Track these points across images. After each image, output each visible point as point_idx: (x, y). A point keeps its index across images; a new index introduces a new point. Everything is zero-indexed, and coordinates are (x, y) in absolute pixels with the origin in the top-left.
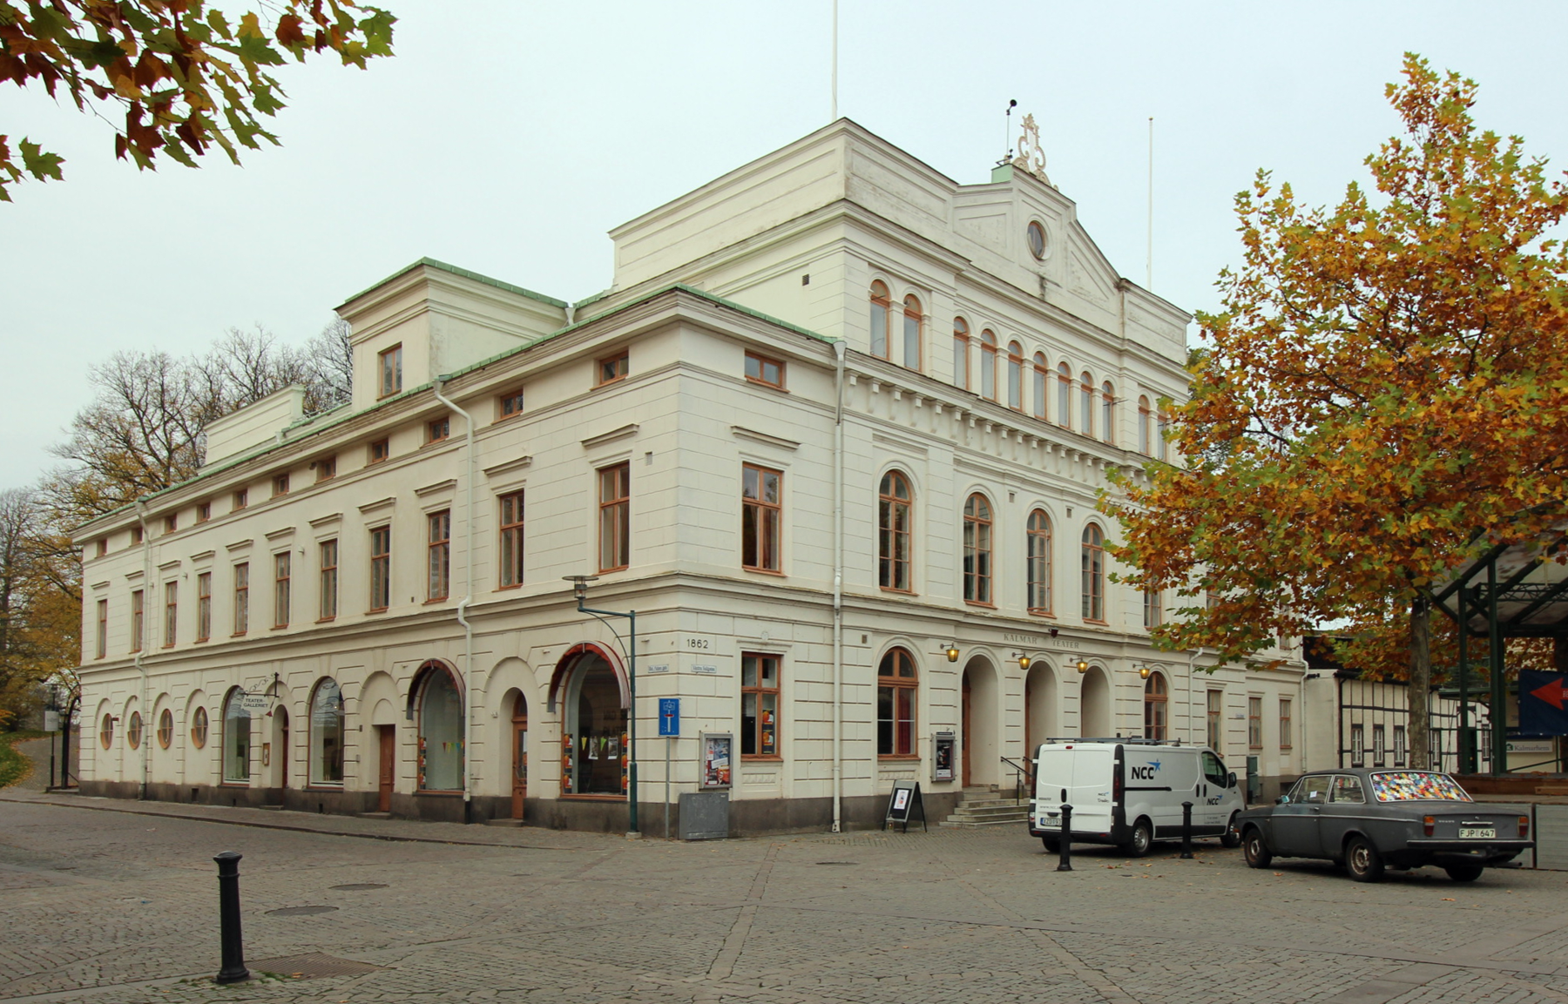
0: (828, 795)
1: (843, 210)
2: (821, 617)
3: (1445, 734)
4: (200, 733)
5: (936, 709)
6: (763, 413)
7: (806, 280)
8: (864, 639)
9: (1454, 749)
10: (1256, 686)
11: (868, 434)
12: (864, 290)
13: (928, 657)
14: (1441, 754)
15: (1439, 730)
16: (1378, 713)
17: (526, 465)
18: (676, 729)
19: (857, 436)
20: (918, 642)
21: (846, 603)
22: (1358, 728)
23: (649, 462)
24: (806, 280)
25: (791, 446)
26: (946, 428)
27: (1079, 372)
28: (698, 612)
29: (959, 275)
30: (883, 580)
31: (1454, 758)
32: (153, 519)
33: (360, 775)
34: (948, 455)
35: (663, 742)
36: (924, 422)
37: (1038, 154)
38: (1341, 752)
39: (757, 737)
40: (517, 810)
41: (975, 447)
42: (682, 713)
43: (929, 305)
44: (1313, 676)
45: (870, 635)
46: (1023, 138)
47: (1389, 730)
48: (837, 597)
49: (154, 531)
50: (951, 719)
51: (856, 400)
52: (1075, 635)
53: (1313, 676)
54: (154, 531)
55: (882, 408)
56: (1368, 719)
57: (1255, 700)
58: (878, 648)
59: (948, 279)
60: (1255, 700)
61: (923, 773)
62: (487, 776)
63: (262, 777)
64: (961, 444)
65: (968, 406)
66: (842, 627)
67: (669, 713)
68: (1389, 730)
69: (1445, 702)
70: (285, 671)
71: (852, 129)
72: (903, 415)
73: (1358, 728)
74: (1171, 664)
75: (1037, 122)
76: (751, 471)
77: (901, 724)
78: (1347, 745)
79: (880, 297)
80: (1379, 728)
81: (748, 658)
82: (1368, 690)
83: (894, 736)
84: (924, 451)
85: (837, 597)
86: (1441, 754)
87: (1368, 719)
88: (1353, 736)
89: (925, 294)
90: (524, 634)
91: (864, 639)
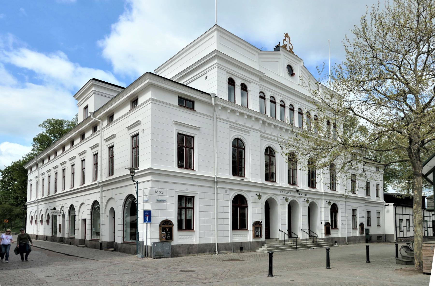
0: (214, 242)
1: (215, 54)
2: (344, 200)
3: (428, 222)
4: (48, 221)
5: (255, 213)
6: (184, 116)
7: (206, 78)
8: (226, 192)
9: (431, 226)
10: (369, 209)
11: (227, 126)
12: (226, 81)
13: (250, 198)
14: (427, 228)
15: (427, 221)
16: (401, 216)
17: (115, 137)
18: (150, 220)
19: (223, 127)
20: (247, 193)
21: (218, 180)
22: (401, 220)
23: (144, 133)
24: (206, 78)
25: (197, 129)
26: (257, 126)
27: (313, 116)
28: (174, 183)
29: (261, 79)
30: (309, 186)
31: (432, 229)
32: (39, 162)
33: (78, 236)
34: (258, 135)
35: (145, 224)
36: (249, 124)
37: (290, 45)
38: (396, 227)
39: (187, 225)
40: (112, 247)
41: (268, 132)
42: (152, 215)
43: (250, 87)
44: (387, 205)
45: (228, 191)
46: (285, 40)
47: (405, 221)
48: (215, 178)
49: (40, 165)
50: (261, 218)
51: (224, 115)
52: (305, 193)
53: (387, 205)
54: (40, 165)
55: (233, 119)
56: (405, 218)
57: (368, 213)
58: (232, 195)
59: (258, 80)
60: (368, 213)
61: (247, 236)
62: (105, 237)
63: (59, 235)
64: (263, 131)
65: (265, 119)
66: (217, 188)
67: (148, 215)
68: (405, 221)
69: (428, 212)
70: (64, 202)
71: (219, 29)
72: (241, 121)
73: (401, 220)
74: (339, 201)
75: (289, 35)
76: (180, 135)
77: (240, 220)
78: (398, 225)
79: (231, 82)
80: (408, 220)
81: (180, 198)
82: (404, 209)
83: (239, 223)
84: (249, 133)
85: (215, 178)
86: (427, 228)
87: (405, 218)
88: (400, 223)
89: (249, 83)
90: (114, 190)
91: (226, 192)
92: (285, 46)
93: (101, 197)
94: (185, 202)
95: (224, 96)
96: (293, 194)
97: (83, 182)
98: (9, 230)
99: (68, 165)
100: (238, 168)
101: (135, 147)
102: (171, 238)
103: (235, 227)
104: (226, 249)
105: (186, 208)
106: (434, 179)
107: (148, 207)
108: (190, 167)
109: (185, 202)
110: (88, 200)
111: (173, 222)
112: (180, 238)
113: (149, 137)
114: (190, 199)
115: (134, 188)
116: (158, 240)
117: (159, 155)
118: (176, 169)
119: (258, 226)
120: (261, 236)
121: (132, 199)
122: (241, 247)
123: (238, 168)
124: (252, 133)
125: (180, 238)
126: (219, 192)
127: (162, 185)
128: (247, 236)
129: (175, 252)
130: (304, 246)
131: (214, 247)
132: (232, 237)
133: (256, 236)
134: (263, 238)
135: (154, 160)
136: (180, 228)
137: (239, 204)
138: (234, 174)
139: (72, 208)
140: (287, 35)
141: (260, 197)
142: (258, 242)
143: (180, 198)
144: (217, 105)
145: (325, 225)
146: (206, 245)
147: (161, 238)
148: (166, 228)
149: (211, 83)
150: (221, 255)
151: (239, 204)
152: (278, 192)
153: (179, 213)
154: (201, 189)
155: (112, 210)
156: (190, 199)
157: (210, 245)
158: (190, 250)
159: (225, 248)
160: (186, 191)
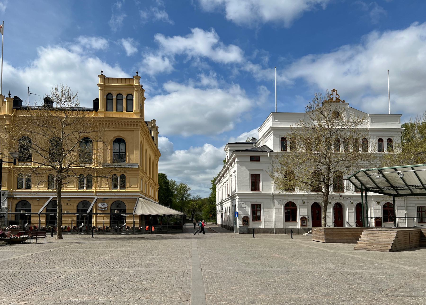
13: (346, 203)
39: (257, 218)
91: (280, 201)
95: (277, 150)
98: (205, 81)
109: (256, 208)
111: (249, 217)
112: (252, 225)
116: (242, 225)
118: (249, 192)
119: (304, 219)
120: (307, 226)
122: (292, 232)
125: (252, 225)
126: (275, 201)
129: (253, 231)
132: (285, 225)
136: (253, 220)
141: (352, 203)
142: (305, 229)
145: (375, 220)
147: (243, 224)
148: (245, 220)
157: (271, 229)
159: (279, 231)
160: (256, 202)
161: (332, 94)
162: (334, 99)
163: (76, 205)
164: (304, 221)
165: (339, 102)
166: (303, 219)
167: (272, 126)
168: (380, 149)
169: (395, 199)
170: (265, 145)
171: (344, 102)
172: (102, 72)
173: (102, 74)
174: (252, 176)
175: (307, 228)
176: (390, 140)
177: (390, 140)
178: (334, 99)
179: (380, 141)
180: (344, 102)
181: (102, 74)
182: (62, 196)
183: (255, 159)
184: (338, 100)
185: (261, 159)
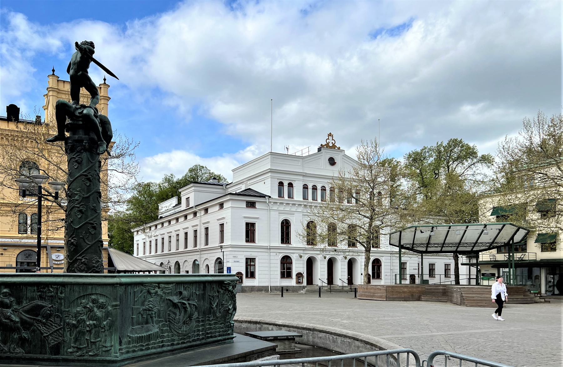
2: (390, 255)
5: (299, 266)
13: (294, 257)
25: (257, 218)
51: (275, 207)
58: (281, 256)
61: (292, 282)
70: (170, 259)
83: (286, 273)
92: (327, 145)
93: (200, 258)
94: (250, 262)
95: (275, 196)
96: (331, 253)
97: (186, 247)
99: (174, 235)
100: (285, 237)
101: (222, 231)
102: (242, 282)
103: (283, 276)
104: (276, 290)
105: (250, 265)
106: (139, 287)
107: (229, 265)
108: (253, 241)
109: (250, 262)
110: (191, 259)
113: (230, 227)
114: (253, 260)
115: (222, 253)
117: (235, 235)
118: (244, 243)
120: (302, 283)
121: (219, 260)
123: (285, 237)
124: (296, 214)
127: (236, 253)
128: (292, 282)
130: (341, 290)
131: (344, 352)
133: (298, 282)
134: (305, 283)
135: (232, 239)
136: (247, 276)
137: (286, 262)
138: (282, 242)
139: (177, 264)
140: (330, 135)
141: (301, 257)
143: (247, 224)
144: (270, 202)
146: (263, 287)
149: (266, 187)
150: (272, 293)
151: (286, 262)
152: (319, 252)
153: (255, 352)
154: (259, 254)
155: (207, 266)
156: (253, 260)
158: (252, 289)
159: (274, 289)
160: (250, 255)
161: (328, 139)
162: (331, 145)
163: (16, 256)
164: (300, 277)
165: (335, 148)
166: (299, 275)
167: (270, 168)
168: (305, 197)
169: (424, 257)
170: (250, 189)
171: (339, 148)
172: (53, 71)
173: (105, 83)
174: (247, 224)
175: (302, 285)
176: (290, 185)
177: (290, 185)
178: (331, 145)
179: (305, 187)
180: (339, 148)
181: (105, 83)
182: (501, 269)
183: (251, 205)
184: (334, 146)
185: (257, 205)
